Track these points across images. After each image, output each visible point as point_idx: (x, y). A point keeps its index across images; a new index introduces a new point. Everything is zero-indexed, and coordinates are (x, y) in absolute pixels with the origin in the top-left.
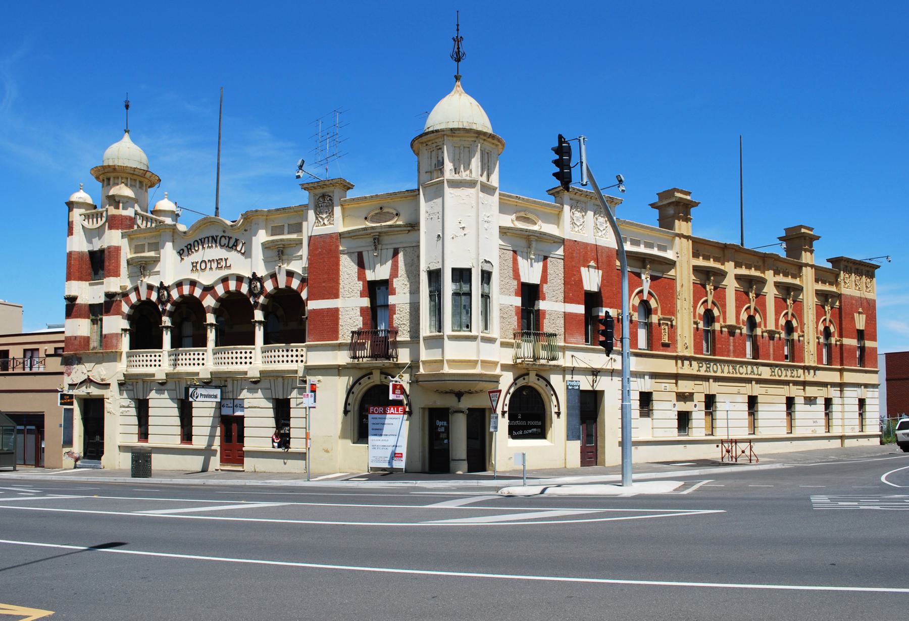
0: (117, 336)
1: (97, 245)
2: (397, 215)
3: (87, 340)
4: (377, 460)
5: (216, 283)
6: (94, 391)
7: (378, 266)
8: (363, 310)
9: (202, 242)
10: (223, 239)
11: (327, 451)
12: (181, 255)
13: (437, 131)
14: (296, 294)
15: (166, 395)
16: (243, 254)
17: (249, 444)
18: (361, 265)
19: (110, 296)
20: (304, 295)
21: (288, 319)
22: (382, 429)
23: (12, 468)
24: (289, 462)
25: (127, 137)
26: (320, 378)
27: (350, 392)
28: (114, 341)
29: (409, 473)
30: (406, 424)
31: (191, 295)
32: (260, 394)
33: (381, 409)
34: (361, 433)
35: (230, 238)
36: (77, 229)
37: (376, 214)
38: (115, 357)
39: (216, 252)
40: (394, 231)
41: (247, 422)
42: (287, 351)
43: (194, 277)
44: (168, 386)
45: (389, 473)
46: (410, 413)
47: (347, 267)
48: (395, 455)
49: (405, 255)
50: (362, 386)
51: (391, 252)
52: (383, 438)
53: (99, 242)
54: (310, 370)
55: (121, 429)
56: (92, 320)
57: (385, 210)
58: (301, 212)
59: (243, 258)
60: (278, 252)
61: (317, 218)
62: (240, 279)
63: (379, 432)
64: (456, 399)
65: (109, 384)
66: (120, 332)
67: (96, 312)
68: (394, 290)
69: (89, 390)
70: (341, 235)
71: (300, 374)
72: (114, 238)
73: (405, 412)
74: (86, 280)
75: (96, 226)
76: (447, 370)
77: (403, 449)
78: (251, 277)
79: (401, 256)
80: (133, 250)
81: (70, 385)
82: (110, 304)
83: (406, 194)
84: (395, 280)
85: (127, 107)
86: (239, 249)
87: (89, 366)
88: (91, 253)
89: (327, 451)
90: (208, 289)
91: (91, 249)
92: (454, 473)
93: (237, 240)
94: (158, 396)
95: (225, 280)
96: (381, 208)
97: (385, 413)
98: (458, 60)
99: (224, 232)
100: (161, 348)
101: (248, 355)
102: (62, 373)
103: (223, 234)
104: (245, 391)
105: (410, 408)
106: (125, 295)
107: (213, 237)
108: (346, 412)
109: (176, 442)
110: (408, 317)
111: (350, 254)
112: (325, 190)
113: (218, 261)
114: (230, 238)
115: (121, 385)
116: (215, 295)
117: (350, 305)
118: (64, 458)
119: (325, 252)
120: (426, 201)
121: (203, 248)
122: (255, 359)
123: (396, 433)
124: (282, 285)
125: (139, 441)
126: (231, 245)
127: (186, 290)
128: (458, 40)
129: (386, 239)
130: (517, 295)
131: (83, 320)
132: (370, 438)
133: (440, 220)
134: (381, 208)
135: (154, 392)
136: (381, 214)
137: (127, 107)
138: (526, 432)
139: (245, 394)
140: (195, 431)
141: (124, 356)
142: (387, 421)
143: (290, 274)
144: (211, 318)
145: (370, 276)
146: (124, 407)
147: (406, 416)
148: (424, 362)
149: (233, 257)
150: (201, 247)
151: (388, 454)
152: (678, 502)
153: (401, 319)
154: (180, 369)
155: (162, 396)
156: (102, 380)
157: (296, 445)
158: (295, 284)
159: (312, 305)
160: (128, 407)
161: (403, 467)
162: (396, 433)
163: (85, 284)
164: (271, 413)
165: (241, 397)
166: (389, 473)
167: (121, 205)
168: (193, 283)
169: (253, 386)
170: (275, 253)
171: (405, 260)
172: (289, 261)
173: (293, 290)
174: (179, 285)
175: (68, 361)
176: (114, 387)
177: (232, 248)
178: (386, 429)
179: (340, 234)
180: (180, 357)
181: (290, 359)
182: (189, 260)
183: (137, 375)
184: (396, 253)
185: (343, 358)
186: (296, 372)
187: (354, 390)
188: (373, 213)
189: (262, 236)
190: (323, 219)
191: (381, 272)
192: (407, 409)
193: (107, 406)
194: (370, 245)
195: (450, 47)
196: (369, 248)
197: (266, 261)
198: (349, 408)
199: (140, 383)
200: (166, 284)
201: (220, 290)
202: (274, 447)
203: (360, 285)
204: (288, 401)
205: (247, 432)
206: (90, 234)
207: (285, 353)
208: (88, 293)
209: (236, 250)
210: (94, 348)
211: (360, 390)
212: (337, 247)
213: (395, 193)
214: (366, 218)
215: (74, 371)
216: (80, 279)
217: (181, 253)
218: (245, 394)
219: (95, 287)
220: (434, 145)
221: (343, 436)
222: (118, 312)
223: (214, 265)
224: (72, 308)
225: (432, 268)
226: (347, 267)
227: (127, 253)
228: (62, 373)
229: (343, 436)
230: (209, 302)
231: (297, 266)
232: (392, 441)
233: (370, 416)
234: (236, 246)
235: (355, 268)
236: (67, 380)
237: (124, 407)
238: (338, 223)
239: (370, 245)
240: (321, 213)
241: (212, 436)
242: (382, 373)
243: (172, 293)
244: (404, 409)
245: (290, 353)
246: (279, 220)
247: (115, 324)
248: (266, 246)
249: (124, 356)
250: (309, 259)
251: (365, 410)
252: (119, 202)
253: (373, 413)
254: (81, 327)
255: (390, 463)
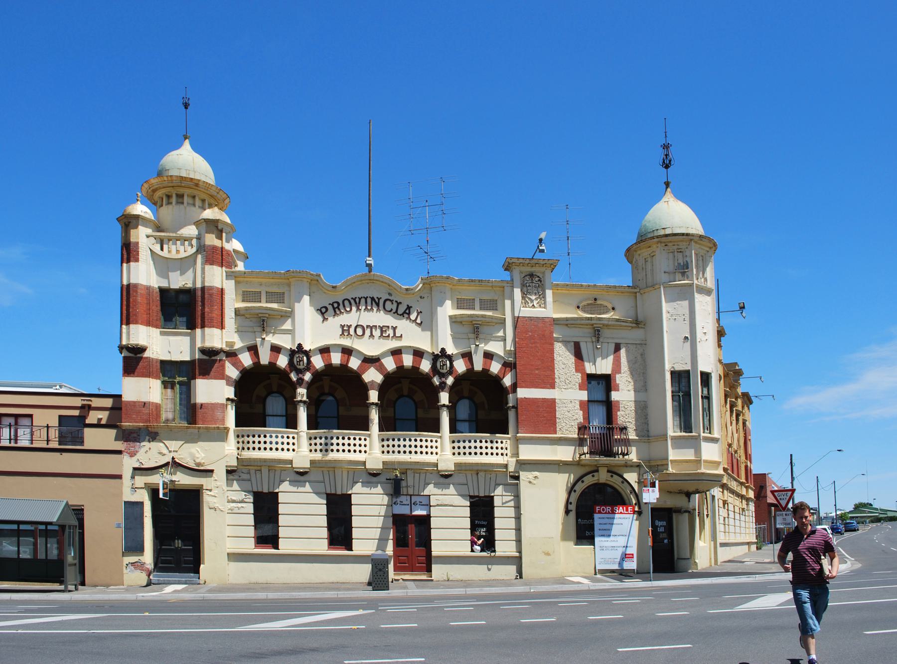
0: (223, 407)
1: (178, 281)
2: (613, 309)
3: (158, 407)
4: (606, 562)
5: (384, 354)
6: (183, 480)
7: (599, 360)
8: (582, 403)
9: (356, 302)
10: (388, 304)
11: (548, 554)
12: (323, 314)
13: (687, 235)
14: (496, 380)
15: (308, 487)
16: (420, 324)
17: (437, 549)
18: (578, 355)
19: (210, 353)
20: (507, 381)
21: (486, 404)
22: (610, 530)
23: (62, 587)
24: (495, 568)
25: (187, 143)
26: (536, 473)
27: (571, 490)
28: (219, 414)
29: (639, 573)
30: (636, 524)
31: (400, 368)
32: (452, 490)
33: (608, 509)
34: (584, 533)
35: (399, 304)
36: (144, 254)
37: (589, 305)
38: (221, 435)
39: (378, 318)
40: (621, 326)
41: (434, 522)
42: (492, 442)
43: (347, 342)
44: (382, 478)
45: (622, 574)
46: (640, 513)
47: (563, 357)
48: (625, 556)
49: (627, 352)
50: (621, 485)
51: (612, 347)
52: (612, 538)
53: (180, 278)
54: (524, 465)
55: (229, 531)
56: (163, 382)
57: (598, 302)
58: (505, 290)
59: (419, 329)
60: (472, 329)
61: (523, 298)
62: (418, 354)
63: (607, 533)
64: (686, 499)
65: (212, 471)
66: (224, 402)
67: (179, 375)
68: (618, 385)
69: (174, 478)
70: (556, 321)
71: (511, 468)
72: (215, 276)
73: (634, 512)
74: (157, 327)
75: (183, 255)
76: (703, 470)
77: (633, 550)
78: (294, 348)
79: (623, 352)
80: (240, 298)
81: (135, 469)
82: (207, 363)
83: (627, 290)
84: (618, 376)
85: (186, 106)
86: (413, 317)
87: (173, 445)
88: (163, 291)
89: (548, 554)
90: (370, 361)
91: (164, 284)
92: (686, 571)
93: (409, 308)
94: (439, 491)
95: (396, 353)
96: (595, 299)
97: (613, 512)
98: (667, 167)
99: (390, 294)
100: (296, 428)
101: (363, 443)
102: (119, 452)
103: (388, 297)
104: (432, 486)
105: (639, 508)
106: (232, 355)
107: (373, 299)
108: (567, 512)
109: (321, 547)
110: (633, 414)
111: (565, 342)
112: (533, 269)
113: (383, 329)
114: (399, 304)
115: (229, 472)
116: (381, 369)
117: (568, 396)
118: (125, 571)
119: (534, 339)
120: (666, 302)
121: (358, 309)
122: (441, 449)
123: (624, 534)
124: (478, 366)
125: (256, 547)
126: (400, 312)
127: (336, 359)
128: (666, 147)
129: (606, 333)
130: (618, 402)
131: (155, 380)
132: (597, 540)
133: (687, 322)
134: (595, 299)
135: (432, 486)
136: (594, 305)
137: (186, 106)
138: (15, 527)
139: (430, 490)
140: (498, 534)
141: (231, 436)
142: (615, 521)
143: (488, 356)
144: (374, 396)
145: (590, 369)
146: (234, 501)
147: (635, 516)
148: (706, 461)
149: (403, 325)
150: (354, 309)
151: (618, 555)
152: (342, 594)
153: (626, 416)
154: (332, 456)
155: (374, 490)
156: (198, 464)
157: (504, 546)
158: (495, 368)
159: (523, 393)
160: (242, 502)
161: (635, 568)
162: (624, 534)
163: (155, 332)
164: (467, 512)
165: (426, 492)
166: (622, 574)
167: (224, 235)
168: (347, 352)
169: (443, 480)
170: (467, 329)
171: (627, 357)
172: (487, 341)
173: (351, 370)
174: (325, 351)
175: (131, 436)
176: (220, 474)
177: (402, 315)
178: (615, 529)
179: (554, 320)
180: (335, 441)
181: (494, 452)
182: (336, 322)
183: (265, 460)
184: (617, 348)
185: (566, 453)
186: (506, 466)
187: (576, 488)
188: (585, 303)
189: (447, 310)
190: (532, 301)
191: (603, 366)
192: (636, 509)
193: (208, 499)
194: (586, 338)
195: (661, 153)
196: (586, 339)
197: (455, 338)
198: (570, 507)
199: (265, 471)
200: (307, 347)
201: (390, 364)
202: (472, 551)
203: (578, 378)
204: (491, 498)
205: (434, 534)
206: (163, 265)
207: (489, 445)
208: (164, 344)
209: (409, 318)
210: (167, 420)
211: (580, 487)
212: (552, 333)
213: (615, 287)
214: (578, 307)
215: (142, 450)
216: (148, 324)
217: (323, 311)
218: (430, 490)
219: (172, 338)
220: (675, 247)
221: (565, 538)
222: (222, 376)
223: (377, 333)
224: (134, 360)
225: (677, 369)
226: (563, 357)
227: (232, 302)
228: (119, 452)
229: (565, 538)
230: (372, 376)
231: (495, 347)
232: (622, 541)
233: (596, 516)
234: (409, 314)
235: (571, 359)
236: (128, 464)
237: (234, 501)
238: (548, 308)
239: (586, 338)
240: (530, 293)
241: (382, 541)
242: (608, 471)
243: (455, 363)
244: (634, 509)
245: (495, 445)
246: (467, 293)
247: (214, 391)
248: (455, 321)
249: (231, 436)
250: (515, 342)
251: (588, 511)
252: (221, 231)
253: (600, 512)
254: (146, 390)
255: (620, 564)
